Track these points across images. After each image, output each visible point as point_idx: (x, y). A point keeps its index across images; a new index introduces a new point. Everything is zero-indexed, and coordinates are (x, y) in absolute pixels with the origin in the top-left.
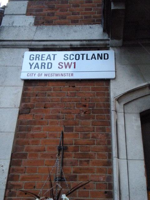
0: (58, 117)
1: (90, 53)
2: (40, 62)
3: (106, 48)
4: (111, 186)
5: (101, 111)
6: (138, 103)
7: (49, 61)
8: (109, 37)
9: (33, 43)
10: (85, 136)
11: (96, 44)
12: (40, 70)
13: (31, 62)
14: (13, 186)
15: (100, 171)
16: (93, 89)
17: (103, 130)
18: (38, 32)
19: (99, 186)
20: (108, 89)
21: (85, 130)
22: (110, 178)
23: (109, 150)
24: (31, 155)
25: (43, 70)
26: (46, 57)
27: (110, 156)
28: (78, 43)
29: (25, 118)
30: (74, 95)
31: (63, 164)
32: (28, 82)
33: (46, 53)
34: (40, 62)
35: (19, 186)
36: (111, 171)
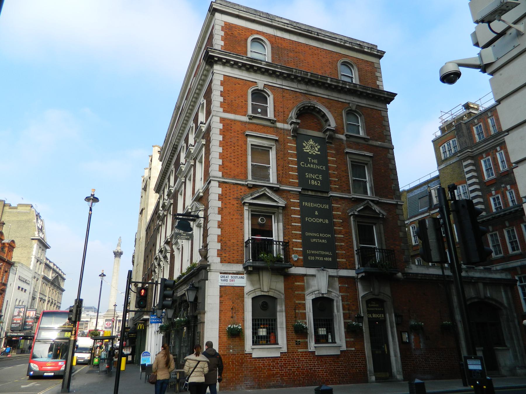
0: (230, 299)
1: (239, 276)
2: (224, 279)
3: (243, 274)
4: (244, 319)
5: (241, 297)
6: (251, 295)
7: (226, 278)
8: (373, 195)
9: (221, 271)
10: (238, 305)
11: (43, 246)
12: (224, 282)
13: (221, 279)
14: (221, 319)
15: (241, 315)
16: (240, 289)
17: (242, 303)
18: (223, 267)
19: (241, 319)
20: (243, 290)
21: (261, 15)
22: (244, 317)
23: (244, 309)
24: (224, 311)
25: (225, 282)
26: (225, 276)
27: (244, 311)
28: (235, 272)
29: (222, 299)
30: (234, 291)
31: (232, 313)
32: (220, 286)
33: (226, 275)
34: (224, 279)
35: (222, 319)
36: (244, 315)
